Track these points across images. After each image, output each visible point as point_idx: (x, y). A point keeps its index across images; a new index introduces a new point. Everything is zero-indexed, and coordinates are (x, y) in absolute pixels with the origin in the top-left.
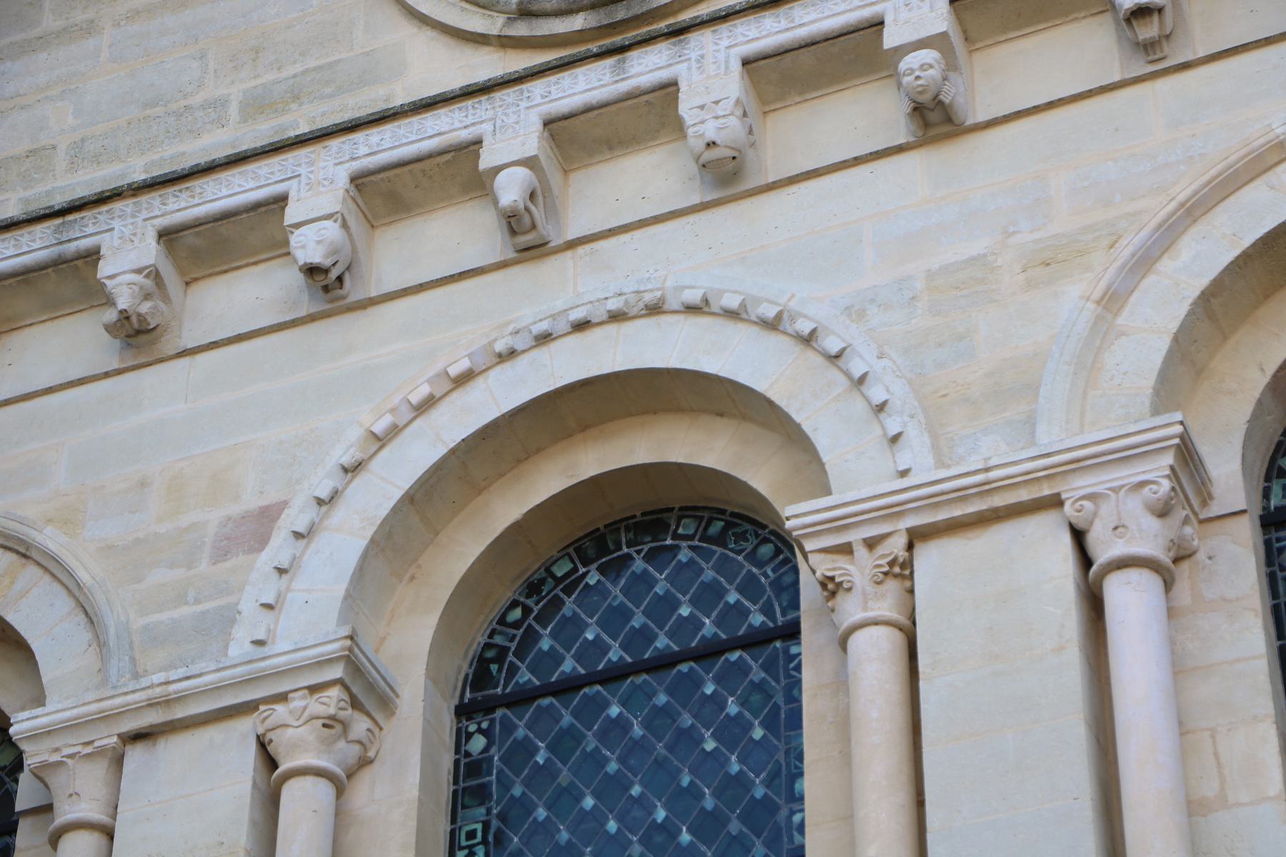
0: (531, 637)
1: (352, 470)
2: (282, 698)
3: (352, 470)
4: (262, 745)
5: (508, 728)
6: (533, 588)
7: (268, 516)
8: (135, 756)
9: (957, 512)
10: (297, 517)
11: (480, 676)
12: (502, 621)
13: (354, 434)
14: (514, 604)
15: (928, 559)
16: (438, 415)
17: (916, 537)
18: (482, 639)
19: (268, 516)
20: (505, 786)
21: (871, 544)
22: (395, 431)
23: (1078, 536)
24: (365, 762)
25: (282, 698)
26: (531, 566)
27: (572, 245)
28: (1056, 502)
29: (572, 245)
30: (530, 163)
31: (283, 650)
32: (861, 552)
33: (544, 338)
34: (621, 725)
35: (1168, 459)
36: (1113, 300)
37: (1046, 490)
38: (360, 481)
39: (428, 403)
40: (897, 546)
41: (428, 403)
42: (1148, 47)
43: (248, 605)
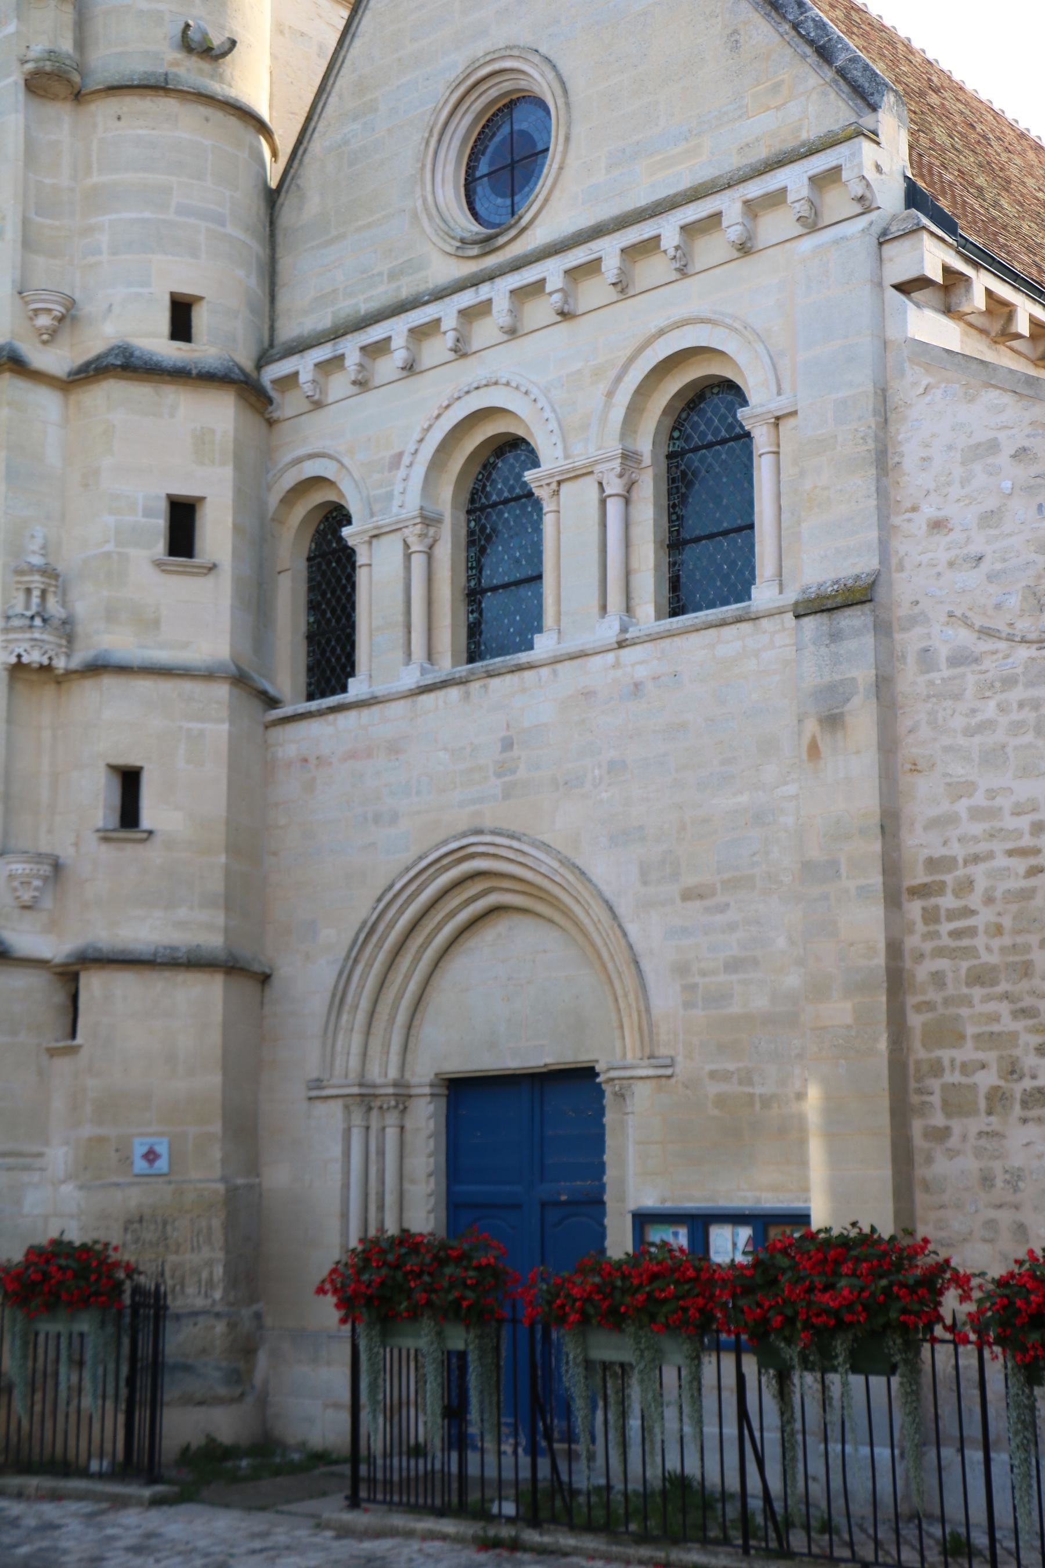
0: (484, 486)
1: (421, 441)
2: (406, 527)
3: (421, 441)
4: (405, 541)
5: (480, 519)
6: (484, 467)
7: (400, 455)
8: (375, 541)
9: (568, 476)
10: (406, 460)
11: (472, 501)
12: (477, 479)
13: (419, 429)
14: (480, 473)
15: (565, 488)
16: (442, 419)
17: (559, 483)
18: (472, 485)
19: (400, 455)
20: (480, 540)
21: (548, 484)
22: (430, 426)
23: (600, 484)
24: (435, 541)
25: (406, 527)
26: (482, 460)
27: (475, 353)
28: (592, 472)
29: (475, 353)
30: (454, 329)
31: (405, 514)
32: (546, 487)
33: (468, 392)
34: (507, 520)
35: (619, 461)
36: (610, 394)
37: (590, 470)
38: (423, 444)
39: (438, 416)
40: (554, 486)
41: (438, 416)
42: (622, 291)
43: (396, 493)
